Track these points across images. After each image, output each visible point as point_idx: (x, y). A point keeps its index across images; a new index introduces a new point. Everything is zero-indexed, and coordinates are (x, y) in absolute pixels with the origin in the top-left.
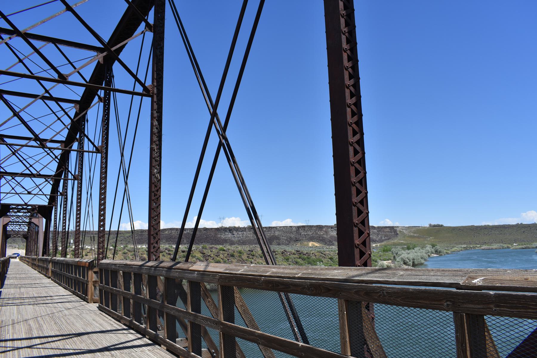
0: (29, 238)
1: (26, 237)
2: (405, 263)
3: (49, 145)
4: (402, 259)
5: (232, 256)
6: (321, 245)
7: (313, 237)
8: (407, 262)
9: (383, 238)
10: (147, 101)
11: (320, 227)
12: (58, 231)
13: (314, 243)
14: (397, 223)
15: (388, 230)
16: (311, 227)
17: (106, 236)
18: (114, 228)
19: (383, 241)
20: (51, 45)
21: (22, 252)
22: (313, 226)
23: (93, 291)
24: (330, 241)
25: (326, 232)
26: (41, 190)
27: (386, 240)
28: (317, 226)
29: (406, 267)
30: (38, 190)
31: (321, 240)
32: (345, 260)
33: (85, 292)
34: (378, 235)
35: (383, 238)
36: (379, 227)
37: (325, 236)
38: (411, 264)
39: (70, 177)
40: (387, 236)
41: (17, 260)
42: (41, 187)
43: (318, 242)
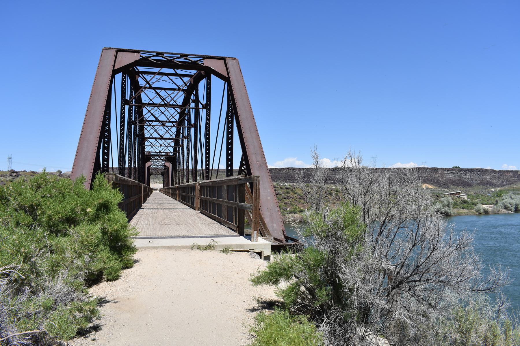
0: (165, 174)
1: (163, 174)
2: (506, 208)
3: (167, 124)
4: (503, 203)
5: (330, 194)
6: (435, 187)
7: (427, 179)
8: (509, 207)
9: (505, 183)
10: (204, 111)
11: (435, 170)
12: (188, 169)
13: (428, 185)
14: (505, 165)
15: (511, 174)
16: (425, 169)
17: (210, 172)
18: (215, 167)
19: (504, 186)
20: (163, 91)
21: (161, 186)
22: (427, 168)
23: (198, 203)
24: (445, 184)
25: (442, 175)
26: (175, 102)
27: (507, 184)
28: (432, 168)
29: (505, 211)
30: (173, 101)
31: (435, 183)
32: (227, 176)
33: (193, 203)
34: (499, 179)
35: (505, 183)
36: (500, 171)
37: (440, 179)
38: (513, 209)
39: (200, 106)
40: (509, 181)
41: (158, 191)
42: (175, 99)
43: (432, 184)
